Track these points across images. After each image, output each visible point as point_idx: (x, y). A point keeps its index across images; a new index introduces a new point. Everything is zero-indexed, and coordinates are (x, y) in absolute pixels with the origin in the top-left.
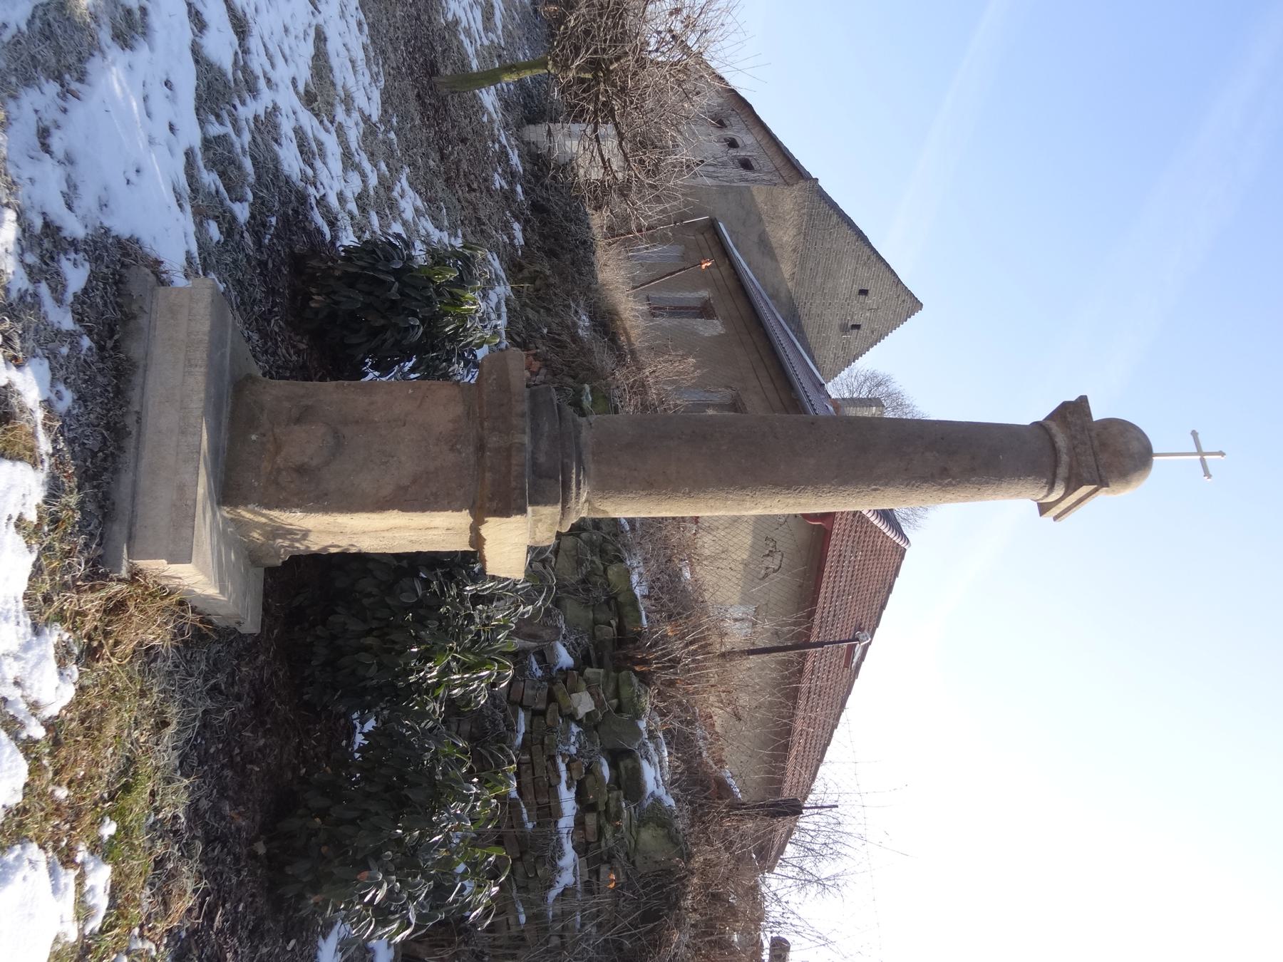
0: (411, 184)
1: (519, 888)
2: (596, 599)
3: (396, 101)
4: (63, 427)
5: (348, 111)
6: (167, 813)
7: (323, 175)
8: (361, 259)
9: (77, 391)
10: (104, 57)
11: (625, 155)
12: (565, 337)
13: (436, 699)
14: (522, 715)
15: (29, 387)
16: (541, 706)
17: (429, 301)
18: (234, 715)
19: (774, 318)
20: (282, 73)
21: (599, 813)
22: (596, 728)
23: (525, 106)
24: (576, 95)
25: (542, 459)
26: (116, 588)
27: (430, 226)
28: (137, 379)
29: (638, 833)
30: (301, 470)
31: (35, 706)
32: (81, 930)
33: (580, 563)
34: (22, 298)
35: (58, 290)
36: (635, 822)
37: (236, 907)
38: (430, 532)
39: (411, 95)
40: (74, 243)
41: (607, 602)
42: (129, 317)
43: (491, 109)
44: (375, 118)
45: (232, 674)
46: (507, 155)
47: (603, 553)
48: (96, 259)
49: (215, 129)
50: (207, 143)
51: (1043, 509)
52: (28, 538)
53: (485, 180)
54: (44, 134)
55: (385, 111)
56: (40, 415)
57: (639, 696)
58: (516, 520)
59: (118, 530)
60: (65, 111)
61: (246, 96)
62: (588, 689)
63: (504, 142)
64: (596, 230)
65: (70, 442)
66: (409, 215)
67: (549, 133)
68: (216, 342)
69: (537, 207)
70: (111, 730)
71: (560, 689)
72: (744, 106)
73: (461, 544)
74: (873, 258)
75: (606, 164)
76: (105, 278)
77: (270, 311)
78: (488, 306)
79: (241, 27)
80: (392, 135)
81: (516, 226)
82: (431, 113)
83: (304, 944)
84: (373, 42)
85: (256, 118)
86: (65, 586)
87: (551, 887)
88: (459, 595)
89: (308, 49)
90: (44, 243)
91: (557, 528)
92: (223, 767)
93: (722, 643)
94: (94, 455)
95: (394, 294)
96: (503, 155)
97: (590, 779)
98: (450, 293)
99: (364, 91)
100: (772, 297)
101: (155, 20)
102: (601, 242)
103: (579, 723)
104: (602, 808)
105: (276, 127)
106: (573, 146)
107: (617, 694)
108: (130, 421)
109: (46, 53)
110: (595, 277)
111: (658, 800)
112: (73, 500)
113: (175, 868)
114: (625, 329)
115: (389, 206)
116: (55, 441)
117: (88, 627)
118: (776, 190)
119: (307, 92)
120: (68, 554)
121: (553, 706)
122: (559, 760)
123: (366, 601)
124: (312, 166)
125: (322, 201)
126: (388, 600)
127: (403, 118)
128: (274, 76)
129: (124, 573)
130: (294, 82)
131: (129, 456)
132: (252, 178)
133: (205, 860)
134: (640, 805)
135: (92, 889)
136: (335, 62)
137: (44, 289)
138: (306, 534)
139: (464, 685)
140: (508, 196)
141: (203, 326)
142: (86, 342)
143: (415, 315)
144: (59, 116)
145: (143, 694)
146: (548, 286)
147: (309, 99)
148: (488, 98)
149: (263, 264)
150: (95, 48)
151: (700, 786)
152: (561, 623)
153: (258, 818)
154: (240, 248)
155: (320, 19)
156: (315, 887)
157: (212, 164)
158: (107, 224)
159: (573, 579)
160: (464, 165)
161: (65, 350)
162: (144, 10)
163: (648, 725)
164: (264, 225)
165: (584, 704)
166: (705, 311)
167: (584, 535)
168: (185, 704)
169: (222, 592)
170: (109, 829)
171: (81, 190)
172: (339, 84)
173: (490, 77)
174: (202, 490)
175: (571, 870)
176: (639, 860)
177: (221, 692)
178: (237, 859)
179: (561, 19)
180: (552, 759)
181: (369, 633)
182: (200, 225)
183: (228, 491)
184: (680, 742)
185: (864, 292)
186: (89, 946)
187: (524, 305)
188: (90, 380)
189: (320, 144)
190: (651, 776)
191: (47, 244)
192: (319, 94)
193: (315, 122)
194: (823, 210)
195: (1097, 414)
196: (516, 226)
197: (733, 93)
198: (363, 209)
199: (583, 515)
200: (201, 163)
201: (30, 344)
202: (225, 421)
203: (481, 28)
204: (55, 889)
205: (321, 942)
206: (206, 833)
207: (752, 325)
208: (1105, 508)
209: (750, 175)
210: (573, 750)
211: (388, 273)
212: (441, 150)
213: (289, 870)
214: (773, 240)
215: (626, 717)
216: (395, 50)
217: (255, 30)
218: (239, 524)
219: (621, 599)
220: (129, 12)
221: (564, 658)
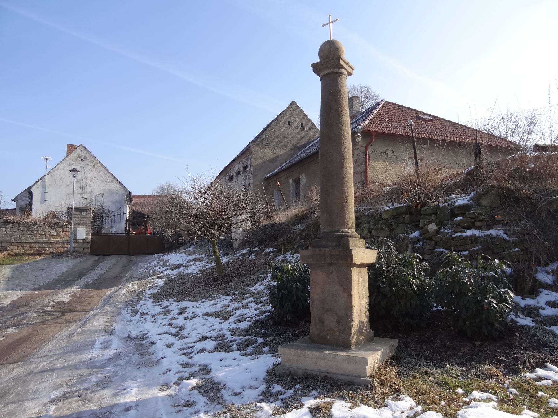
0: (253, 287)
1: (504, 251)
2: (395, 222)
3: (226, 291)
4: (324, 394)
5: (229, 306)
6: (459, 373)
7: (249, 315)
8: (275, 303)
9: (312, 390)
10: (213, 377)
11: (242, 213)
12: (304, 234)
13: (424, 280)
14: (436, 250)
15: (309, 402)
16: (433, 242)
17: (288, 281)
18: (427, 350)
19: (300, 156)
20: (218, 327)
21: (475, 221)
22: (442, 222)
23: (227, 247)
24: (222, 231)
25: (334, 244)
26: (375, 382)
27: (267, 280)
28: (309, 372)
29: (483, 206)
30: (339, 322)
31: (411, 408)
32: (495, 401)
33: (382, 229)
34: (283, 403)
35: (281, 393)
36: (479, 208)
37: (499, 352)
38: (360, 281)
39: (224, 286)
40: (267, 388)
41: (396, 218)
42: (290, 374)
43: (228, 259)
44: (231, 298)
45: (413, 350)
46: (243, 254)
47: (379, 221)
48: (272, 382)
49: (235, 347)
50: (239, 350)
51: (350, 74)
52: (356, 406)
53: (251, 261)
54: (235, 394)
55: (229, 295)
56: (318, 400)
57: (430, 207)
58: (354, 253)
59: (357, 380)
60: (229, 388)
61: (224, 338)
62: (427, 225)
63: (239, 255)
64: (268, 223)
65: (328, 393)
66: (262, 287)
67: (235, 239)
68: (298, 347)
69: (261, 243)
70: (424, 387)
71: (427, 236)
72: (226, 170)
73: (365, 272)
74: (277, 120)
75: (245, 220)
76: (278, 380)
77: (292, 333)
78: (292, 260)
79: (204, 338)
80: (237, 292)
81: (267, 250)
82: (230, 279)
83: (518, 330)
84: (207, 298)
85: (231, 335)
86: (373, 397)
87: (504, 239)
88: (387, 271)
89: (210, 319)
90: (267, 396)
91: (359, 239)
92: (446, 354)
93: (413, 175)
94: (332, 386)
95: (285, 292)
96: (242, 255)
97: (461, 224)
98: (286, 273)
99: (223, 301)
100: (292, 157)
101: (203, 363)
102: (272, 221)
103: (440, 229)
104: (473, 220)
105: (234, 329)
106: (239, 231)
107: (430, 215)
108: (322, 375)
109: (212, 393)
110: (284, 223)
111: (471, 199)
112: (346, 393)
113: (480, 372)
114: (302, 212)
115: (259, 294)
116: (327, 397)
117: (388, 391)
118: (254, 157)
119: (223, 319)
120: (363, 396)
121: (433, 238)
122: (454, 236)
123: (389, 304)
124: (246, 318)
125: (257, 315)
126: (388, 296)
127: (231, 289)
128: (218, 329)
129: (371, 379)
130: (220, 323)
131: (334, 376)
132: (250, 337)
133: (479, 362)
134: (473, 205)
135: (480, 397)
136: (214, 310)
137: (281, 397)
138: (361, 322)
139: (419, 271)
140: (257, 253)
141: (293, 351)
142: (297, 386)
143: (292, 285)
144: (230, 390)
145: (414, 378)
146: (287, 239)
147: (225, 319)
148: (224, 260)
149: (277, 334)
150: (211, 379)
151: (468, 182)
152: (402, 235)
153: (466, 343)
154: (271, 341)
155: (201, 314)
156: (492, 325)
157: (245, 348)
158: (262, 379)
159: (387, 232)
160: (247, 268)
161: (299, 392)
162: (200, 366)
163: (442, 203)
164: (264, 334)
165: (433, 227)
166: (297, 181)
167: (372, 227)
168: (420, 365)
169: (380, 350)
170: (460, 391)
171: (252, 385)
172: (221, 309)
173: (218, 260)
174: (344, 354)
175: (497, 231)
176: (494, 206)
177: (419, 354)
178: (480, 351)
179: (199, 236)
180: (453, 238)
181: (400, 303)
182: (264, 353)
183: (346, 346)
184: (449, 190)
185: (289, 123)
186: (501, 400)
187: (293, 248)
188: (309, 386)
189: (240, 315)
190: (460, 202)
191: (268, 395)
192: (224, 315)
193: (232, 317)
194: (261, 139)
195: (318, 60)
196: (267, 250)
197: (220, 174)
198: (260, 302)
199: (354, 230)
200: (245, 352)
201: (297, 401)
202: (324, 346)
203: (202, 262)
204: (476, 407)
205: (518, 324)
206: (469, 361)
207: (301, 164)
208: (348, 55)
209: (249, 166)
210: (450, 231)
211: (279, 294)
212: (242, 276)
213: (486, 333)
214: (271, 157)
215: (438, 211)
216: (210, 291)
217: (205, 334)
218: (357, 343)
219: (395, 214)
220: (200, 370)
221: (416, 234)
